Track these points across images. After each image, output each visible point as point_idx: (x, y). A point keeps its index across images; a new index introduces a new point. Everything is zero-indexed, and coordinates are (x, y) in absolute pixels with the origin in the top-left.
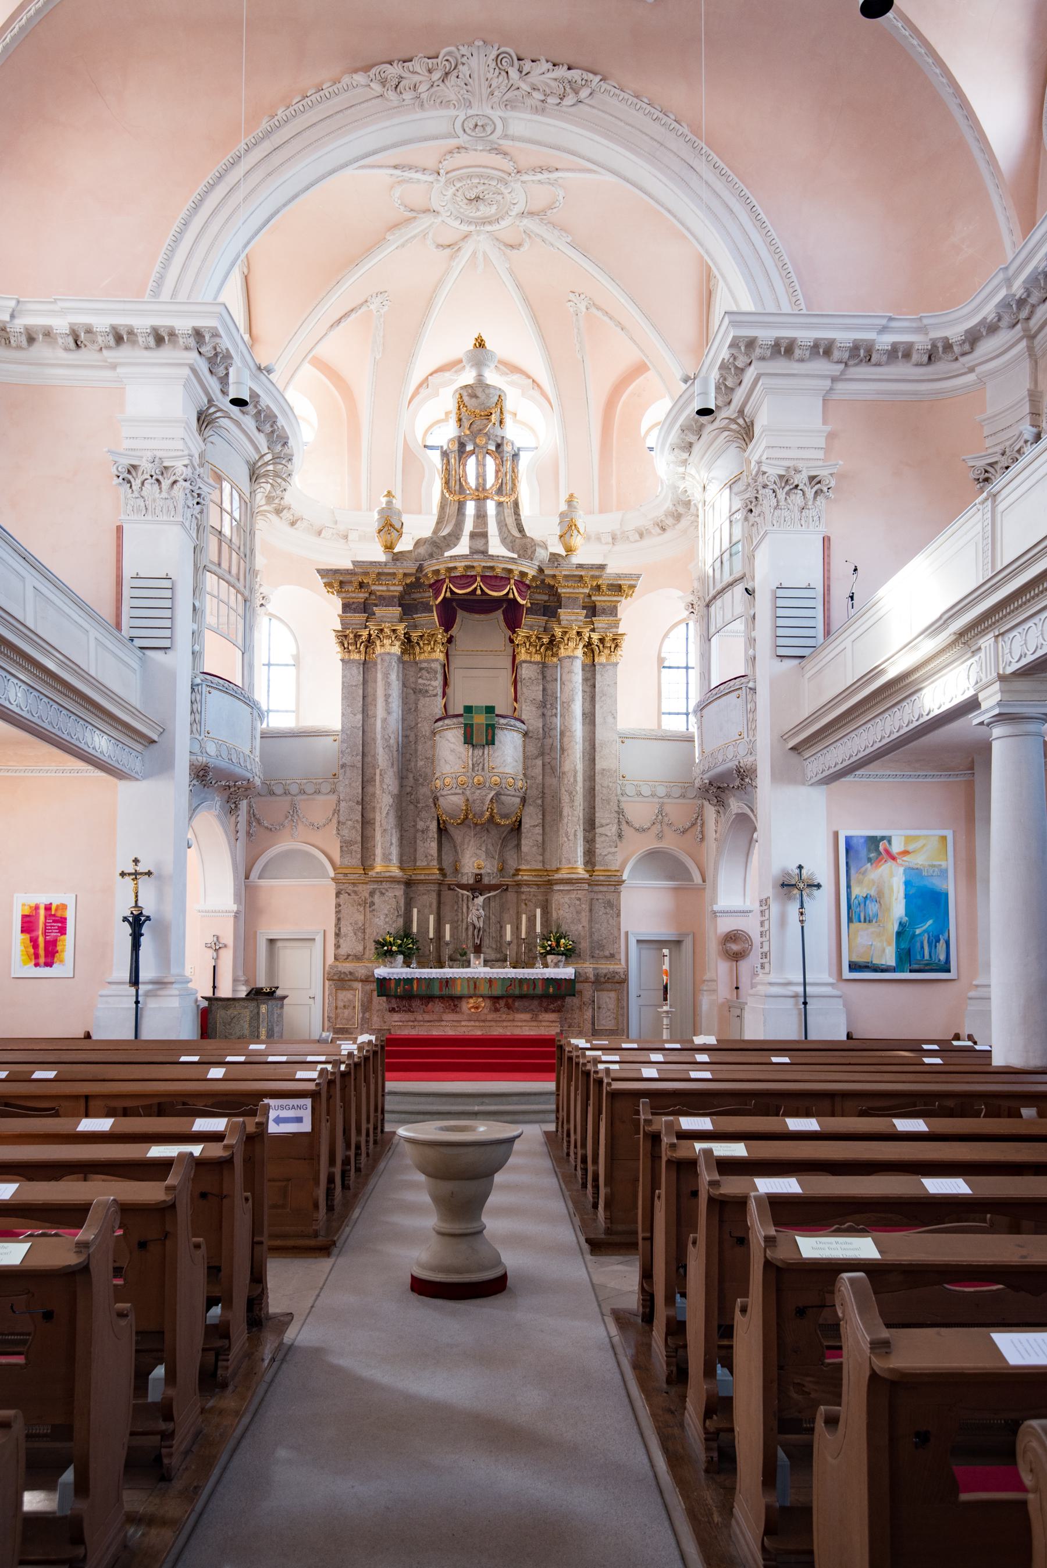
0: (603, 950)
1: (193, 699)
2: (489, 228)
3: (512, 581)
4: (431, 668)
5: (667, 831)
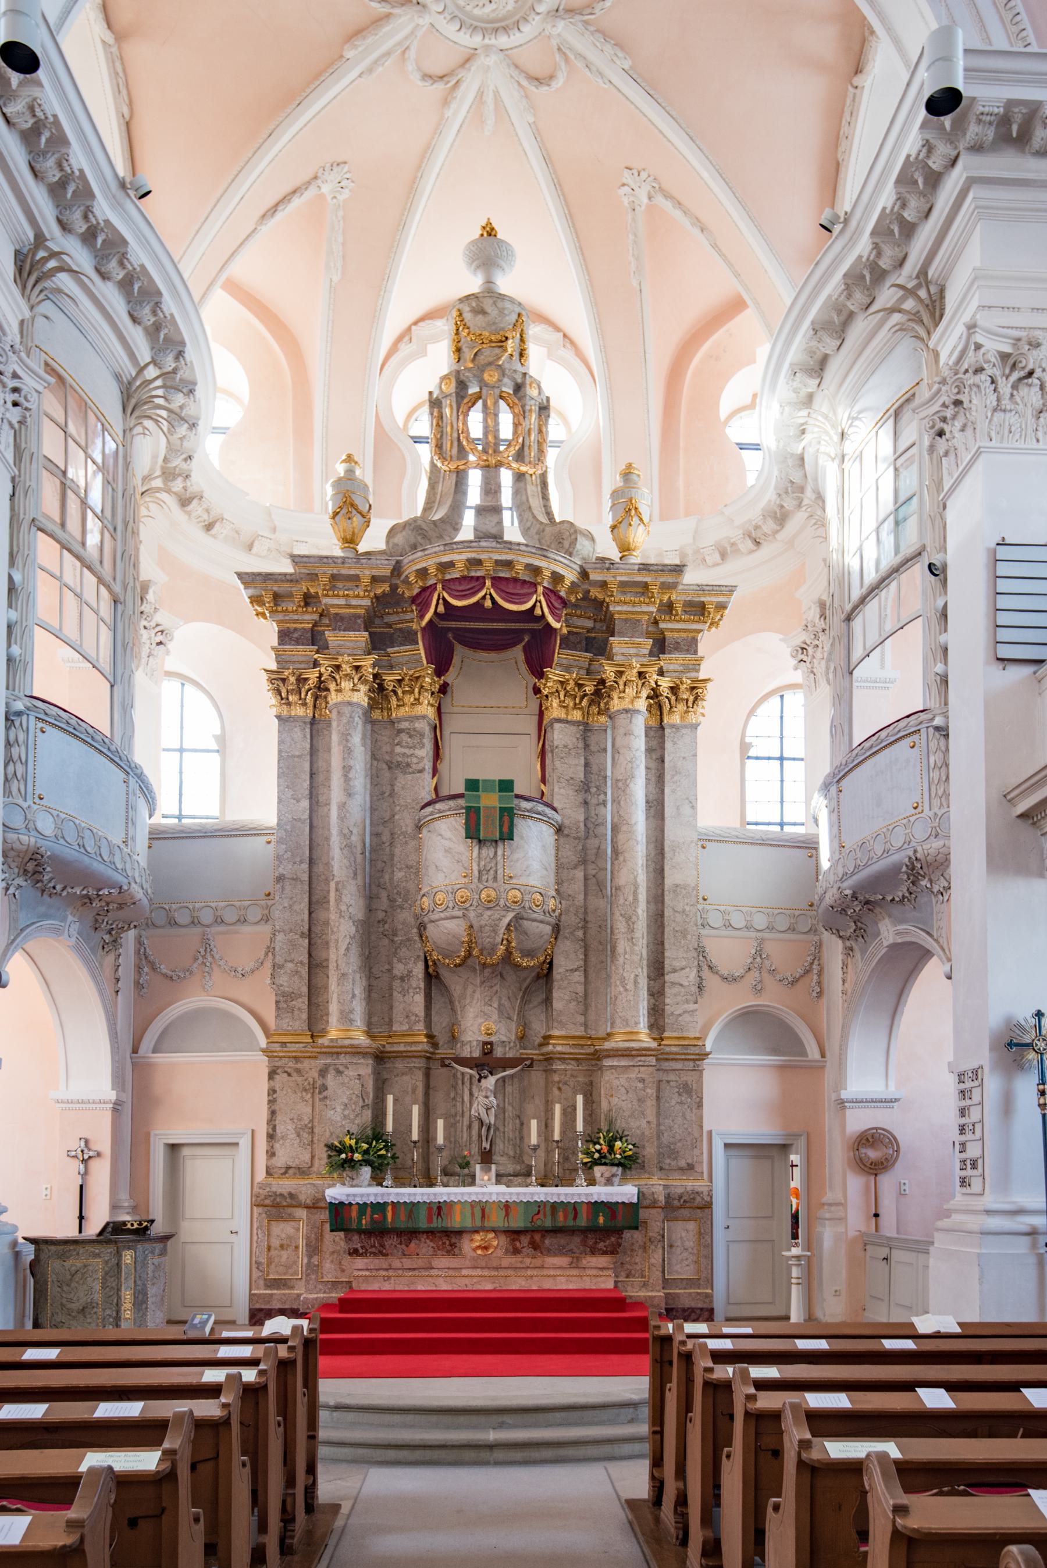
0: (676, 1158)
1: (12, 738)
2: (503, 41)
3: (540, 589)
4: (415, 730)
5: (769, 982)
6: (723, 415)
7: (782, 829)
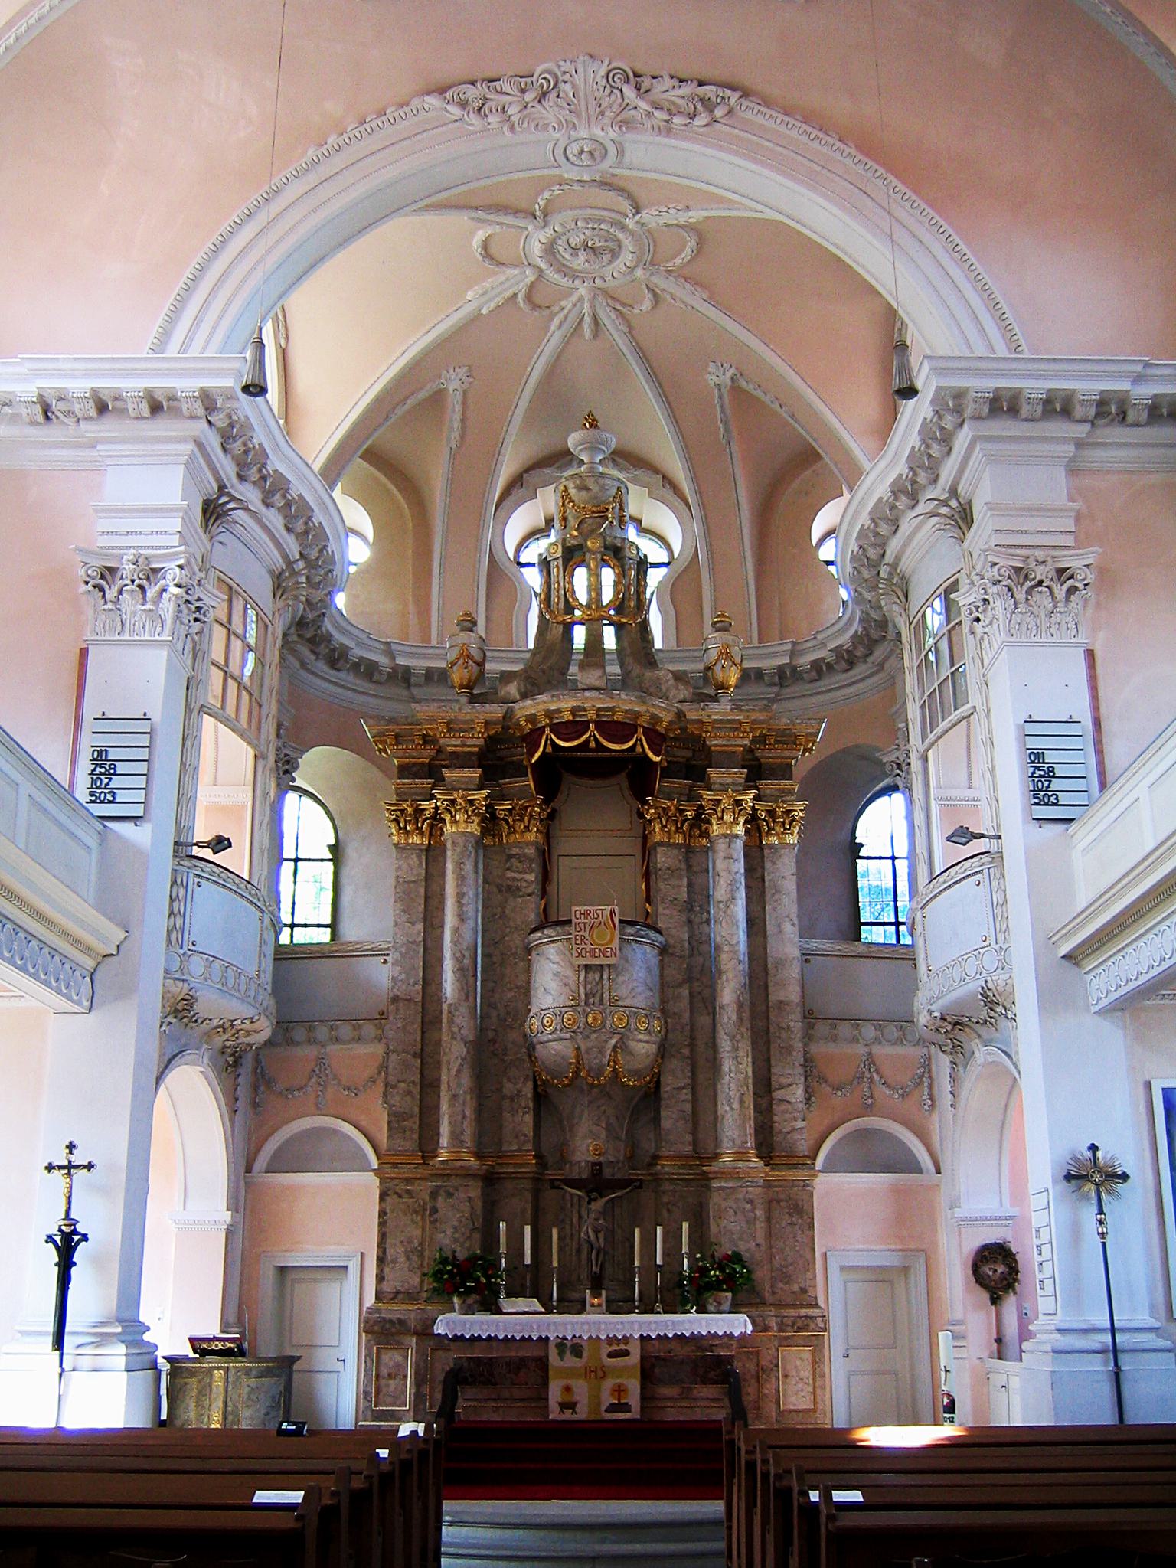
0: (786, 1283)
1: (174, 895)
3: (640, 730)
4: (525, 855)
6: (814, 543)
7: (903, 923)
